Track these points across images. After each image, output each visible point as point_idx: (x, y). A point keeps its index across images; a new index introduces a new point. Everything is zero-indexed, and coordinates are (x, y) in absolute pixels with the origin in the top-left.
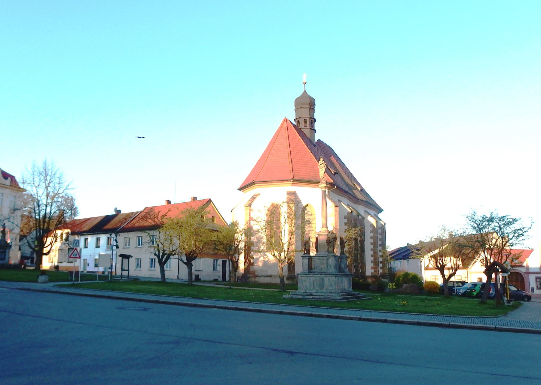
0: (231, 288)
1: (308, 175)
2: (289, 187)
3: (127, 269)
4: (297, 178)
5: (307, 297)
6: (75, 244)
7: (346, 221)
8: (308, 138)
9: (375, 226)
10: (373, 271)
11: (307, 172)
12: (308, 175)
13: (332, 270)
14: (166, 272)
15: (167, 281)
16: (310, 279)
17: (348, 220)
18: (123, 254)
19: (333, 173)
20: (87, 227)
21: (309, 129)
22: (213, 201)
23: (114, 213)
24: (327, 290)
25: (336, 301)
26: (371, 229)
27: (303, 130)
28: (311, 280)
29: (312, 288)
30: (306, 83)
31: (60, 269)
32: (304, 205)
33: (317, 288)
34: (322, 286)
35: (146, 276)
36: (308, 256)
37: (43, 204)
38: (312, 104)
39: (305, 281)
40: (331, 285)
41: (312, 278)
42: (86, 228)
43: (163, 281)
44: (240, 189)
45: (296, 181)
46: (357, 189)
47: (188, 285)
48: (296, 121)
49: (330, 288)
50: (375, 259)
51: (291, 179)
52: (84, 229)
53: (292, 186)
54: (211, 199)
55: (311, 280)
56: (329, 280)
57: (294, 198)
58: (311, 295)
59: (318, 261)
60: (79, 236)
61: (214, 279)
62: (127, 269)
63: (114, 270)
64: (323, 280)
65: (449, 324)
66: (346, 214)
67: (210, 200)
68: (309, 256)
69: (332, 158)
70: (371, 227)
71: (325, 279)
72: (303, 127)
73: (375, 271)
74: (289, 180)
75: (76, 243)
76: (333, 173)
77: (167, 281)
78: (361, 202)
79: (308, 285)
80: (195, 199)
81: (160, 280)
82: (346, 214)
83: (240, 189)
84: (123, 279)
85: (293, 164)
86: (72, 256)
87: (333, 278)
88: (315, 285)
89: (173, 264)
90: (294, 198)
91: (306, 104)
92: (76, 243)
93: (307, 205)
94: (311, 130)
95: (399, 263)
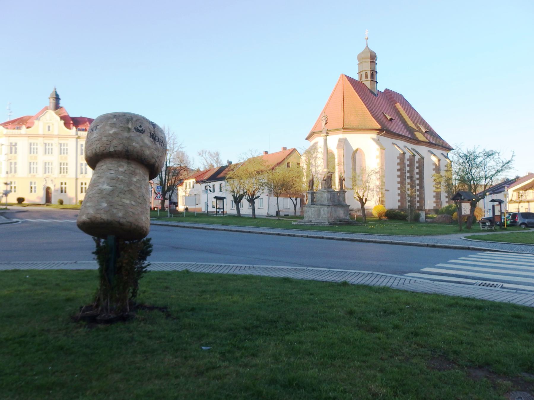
0: (279, 220)
1: (357, 123)
2: (341, 135)
3: (222, 208)
4: (347, 127)
5: (306, 223)
6: (158, 189)
7: (398, 161)
8: (369, 89)
9: (437, 165)
10: (399, 204)
11: (357, 121)
12: (357, 123)
13: (326, 202)
14: (240, 210)
15: (256, 217)
16: (312, 209)
17: (400, 160)
18: (217, 196)
19: (389, 119)
20: (207, 177)
21: (370, 81)
22: (297, 150)
23: (227, 164)
24: (322, 218)
25: (323, 226)
26: (434, 167)
27: (364, 82)
28: (312, 210)
29: (313, 217)
30: (367, 39)
31: (189, 210)
32: (354, 149)
33: (316, 216)
34: (319, 215)
35: (246, 213)
36: (311, 192)
37: (496, 153)
38: (373, 58)
39: (308, 211)
40: (325, 214)
41: (313, 209)
42: (206, 177)
43: (239, 215)
44: (307, 139)
45: (346, 129)
46: (421, 131)
47: (251, 218)
48: (359, 74)
49: (324, 216)
50: (401, 192)
51: (341, 128)
52: (205, 178)
53: (343, 134)
54: (296, 148)
55: (312, 210)
56: (323, 210)
57: (344, 143)
58: (311, 222)
59: (319, 195)
60: (201, 184)
61: (285, 215)
62: (222, 208)
63: (225, 210)
64: (320, 210)
65: (469, 247)
66: (399, 156)
67: (294, 150)
68: (312, 191)
69: (398, 105)
70: (433, 165)
71: (321, 210)
72: (364, 79)
73: (437, 205)
74: (340, 129)
75: (159, 189)
76: (389, 119)
77: (242, 216)
78: (422, 143)
79: (310, 214)
80: (285, 149)
81: (236, 215)
82: (399, 156)
83: (307, 139)
84: (218, 215)
85: (345, 115)
86: (157, 198)
87: (326, 209)
88: (315, 215)
89: (245, 204)
90: (344, 143)
91: (367, 58)
92: (159, 189)
93: (357, 150)
94: (372, 82)
95: (496, 196)
